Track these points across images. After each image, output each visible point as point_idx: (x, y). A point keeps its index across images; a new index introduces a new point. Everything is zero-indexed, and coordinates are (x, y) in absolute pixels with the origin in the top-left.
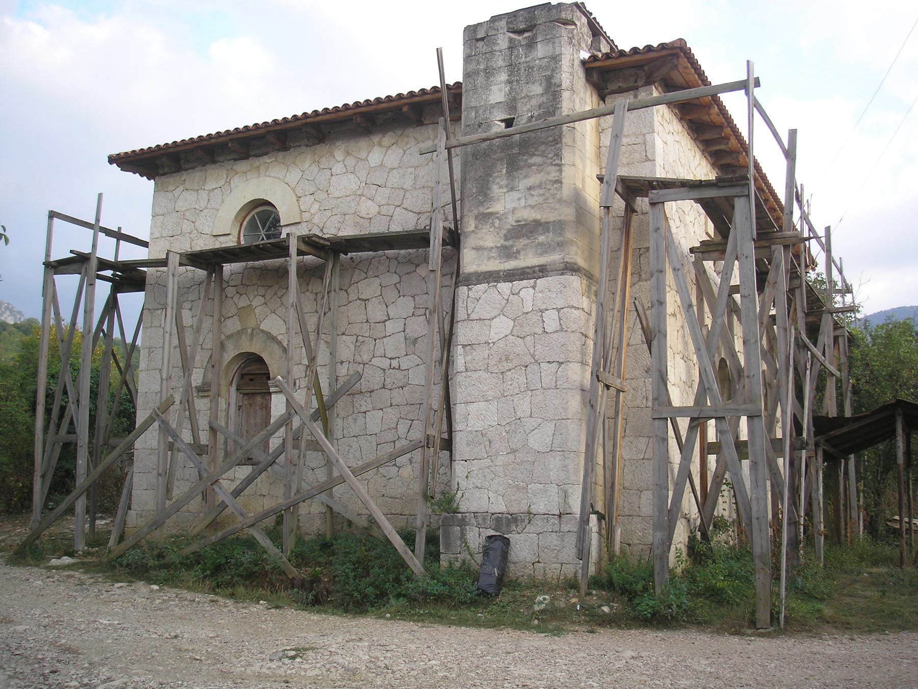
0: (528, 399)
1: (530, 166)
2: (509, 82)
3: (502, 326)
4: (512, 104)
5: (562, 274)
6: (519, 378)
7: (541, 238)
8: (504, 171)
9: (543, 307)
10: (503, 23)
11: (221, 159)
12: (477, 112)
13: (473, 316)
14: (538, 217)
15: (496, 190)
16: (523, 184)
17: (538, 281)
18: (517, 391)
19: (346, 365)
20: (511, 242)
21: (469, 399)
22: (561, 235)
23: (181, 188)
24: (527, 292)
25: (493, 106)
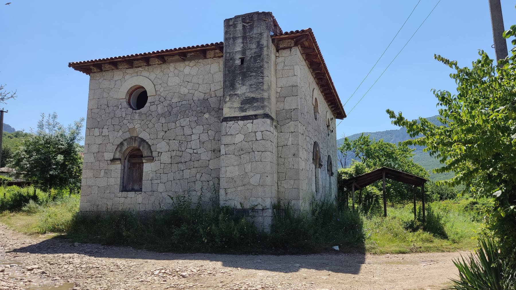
0: (250, 165)
1: (251, 76)
2: (243, 43)
3: (240, 138)
4: (244, 52)
6: (246, 157)
7: (255, 104)
10: (241, 19)
11: (121, 68)
12: (230, 54)
13: (228, 134)
14: (254, 96)
15: (238, 86)
16: (248, 83)
17: (254, 121)
19: (175, 152)
21: (227, 165)
22: (263, 103)
23: (102, 79)
25: (236, 52)
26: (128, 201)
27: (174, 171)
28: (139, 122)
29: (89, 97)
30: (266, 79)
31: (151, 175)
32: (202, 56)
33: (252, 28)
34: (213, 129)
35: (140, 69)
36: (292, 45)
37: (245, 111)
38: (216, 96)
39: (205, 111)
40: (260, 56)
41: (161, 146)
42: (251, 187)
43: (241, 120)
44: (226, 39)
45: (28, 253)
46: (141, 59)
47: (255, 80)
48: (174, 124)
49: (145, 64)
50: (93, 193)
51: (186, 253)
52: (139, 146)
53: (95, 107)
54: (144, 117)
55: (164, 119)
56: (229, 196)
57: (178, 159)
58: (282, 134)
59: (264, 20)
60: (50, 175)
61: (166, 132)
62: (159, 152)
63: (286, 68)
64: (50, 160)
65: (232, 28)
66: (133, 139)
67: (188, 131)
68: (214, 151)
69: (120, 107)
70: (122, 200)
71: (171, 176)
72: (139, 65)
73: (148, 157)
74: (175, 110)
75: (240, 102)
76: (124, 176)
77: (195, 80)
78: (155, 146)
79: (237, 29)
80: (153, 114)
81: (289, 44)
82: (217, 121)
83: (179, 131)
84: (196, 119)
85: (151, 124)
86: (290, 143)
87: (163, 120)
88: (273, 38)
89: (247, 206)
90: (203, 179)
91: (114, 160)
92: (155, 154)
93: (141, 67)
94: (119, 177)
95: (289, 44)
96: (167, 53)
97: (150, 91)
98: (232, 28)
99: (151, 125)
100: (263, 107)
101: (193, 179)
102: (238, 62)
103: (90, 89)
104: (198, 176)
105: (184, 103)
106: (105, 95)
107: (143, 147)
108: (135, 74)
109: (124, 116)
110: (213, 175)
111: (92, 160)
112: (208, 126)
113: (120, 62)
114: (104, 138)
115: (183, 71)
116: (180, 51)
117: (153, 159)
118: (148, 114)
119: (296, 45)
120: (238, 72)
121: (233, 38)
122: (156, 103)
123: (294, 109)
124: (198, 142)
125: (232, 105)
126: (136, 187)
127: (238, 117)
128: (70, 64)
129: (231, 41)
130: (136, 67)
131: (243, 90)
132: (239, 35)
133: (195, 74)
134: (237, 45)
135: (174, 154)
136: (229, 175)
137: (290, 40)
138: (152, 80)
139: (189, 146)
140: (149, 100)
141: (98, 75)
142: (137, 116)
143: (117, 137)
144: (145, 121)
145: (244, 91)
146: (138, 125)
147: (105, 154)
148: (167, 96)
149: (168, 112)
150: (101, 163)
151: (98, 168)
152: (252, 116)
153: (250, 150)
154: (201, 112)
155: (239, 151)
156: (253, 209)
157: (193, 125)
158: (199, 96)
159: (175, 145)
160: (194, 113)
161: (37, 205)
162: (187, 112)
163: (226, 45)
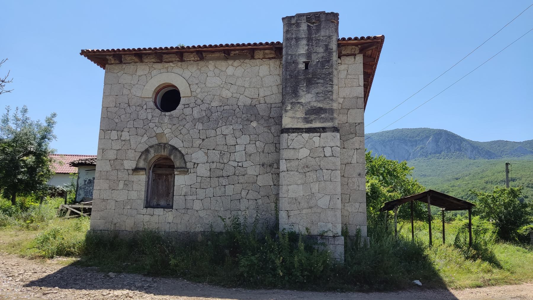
0: (317, 185)
1: (318, 83)
2: (308, 45)
3: (304, 153)
4: (309, 55)
5: (333, 132)
6: (312, 176)
7: (323, 116)
8: (305, 85)
9: (324, 146)
10: (305, 17)
11: (146, 61)
12: (292, 56)
13: (290, 147)
14: (321, 106)
15: (301, 93)
16: (314, 91)
17: (322, 134)
18: (312, 181)
19: (215, 164)
20: (308, 116)
21: (289, 183)
22: (332, 115)
23: (122, 72)
24: (315, 138)
25: (299, 55)
26: (155, 219)
27: (213, 185)
28: (170, 126)
29: (104, 93)
30: (335, 88)
31: (184, 190)
32: (249, 56)
33: (318, 30)
34: (262, 140)
35: (171, 64)
36: (357, 52)
37: (310, 122)
38: (265, 103)
39: (252, 119)
40: (328, 61)
41: (198, 156)
42: (319, 210)
43: (306, 132)
44: (287, 39)
45: (57, 288)
46: (176, 53)
47: (322, 88)
48: (213, 131)
49: (178, 59)
50: (108, 207)
51: (259, 289)
52: (170, 155)
53: (112, 105)
54: (175, 121)
55: (201, 125)
56: (293, 220)
57: (220, 173)
58: (345, 150)
59: (332, 22)
60: (18, 179)
61: (203, 140)
62: (195, 163)
63: (350, 77)
64: (17, 163)
65: (294, 28)
66: (165, 146)
67: (231, 141)
68: (263, 165)
69: (145, 107)
70: (147, 218)
71: (210, 192)
72: (170, 59)
73: (181, 168)
74: (215, 116)
75: (304, 112)
76: (148, 190)
77: (239, 83)
78: (190, 155)
79: (301, 29)
80: (187, 119)
81: (353, 50)
82: (266, 130)
83: (220, 140)
84: (241, 127)
85: (184, 129)
86: (354, 161)
87: (200, 126)
88: (339, 42)
89: (315, 231)
90: (250, 196)
91: (136, 170)
92: (189, 165)
93: (172, 62)
94: (144, 190)
95: (353, 50)
96: (210, 49)
97: (184, 90)
98: (294, 28)
99: (184, 131)
100: (332, 119)
101: (238, 197)
102: (302, 66)
103: (105, 84)
104: (244, 193)
105: (226, 107)
106: (126, 92)
107: (175, 156)
108: (165, 70)
109: (150, 117)
110: (262, 193)
111: (108, 168)
112: (256, 136)
113: (149, 54)
114: (123, 143)
115: (225, 71)
116: (227, 48)
117: (188, 171)
118: (180, 118)
119: (361, 51)
120: (302, 77)
121: (295, 38)
122: (191, 105)
123: (359, 124)
124: (244, 154)
125: (294, 115)
126: (162, 203)
127: (303, 129)
128: (83, 51)
129: (293, 42)
130: (166, 62)
131: (307, 98)
132: (304, 36)
133: (240, 75)
134: (300, 47)
135: (214, 166)
136: (291, 195)
137: (354, 47)
138: (187, 78)
139: (233, 158)
140: (183, 101)
141: (117, 68)
142: (166, 120)
143: (142, 143)
144: (178, 125)
145: (309, 100)
146: (168, 129)
147: (125, 162)
148: (206, 98)
149: (206, 117)
150: (119, 173)
151: (116, 178)
152: (318, 128)
153: (318, 168)
154: (248, 120)
155: (304, 167)
156: (322, 236)
157: (238, 134)
158: (244, 101)
159: (215, 155)
160: (239, 120)
161: (7, 216)
162: (230, 118)
163: (287, 46)
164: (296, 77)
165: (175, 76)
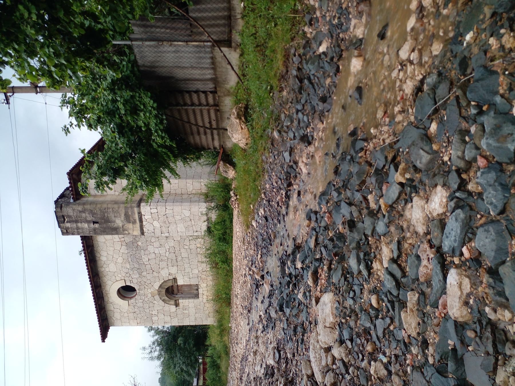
2: (81, 222)
3: (156, 224)
4: (88, 222)
6: (171, 219)
7: (130, 213)
15: (116, 225)
26: (205, 293)
27: (183, 264)
39: (136, 245)
54: (142, 287)
71: (187, 266)
74: (136, 266)
79: (70, 226)
87: (144, 274)
91: (177, 305)
92: (171, 277)
99: (148, 282)
102: (97, 226)
104: (186, 247)
105: (130, 260)
132: (75, 225)
135: (170, 264)
142: (142, 292)
157: (147, 252)
162: (137, 257)
164: (105, 228)
165: (111, 290)
